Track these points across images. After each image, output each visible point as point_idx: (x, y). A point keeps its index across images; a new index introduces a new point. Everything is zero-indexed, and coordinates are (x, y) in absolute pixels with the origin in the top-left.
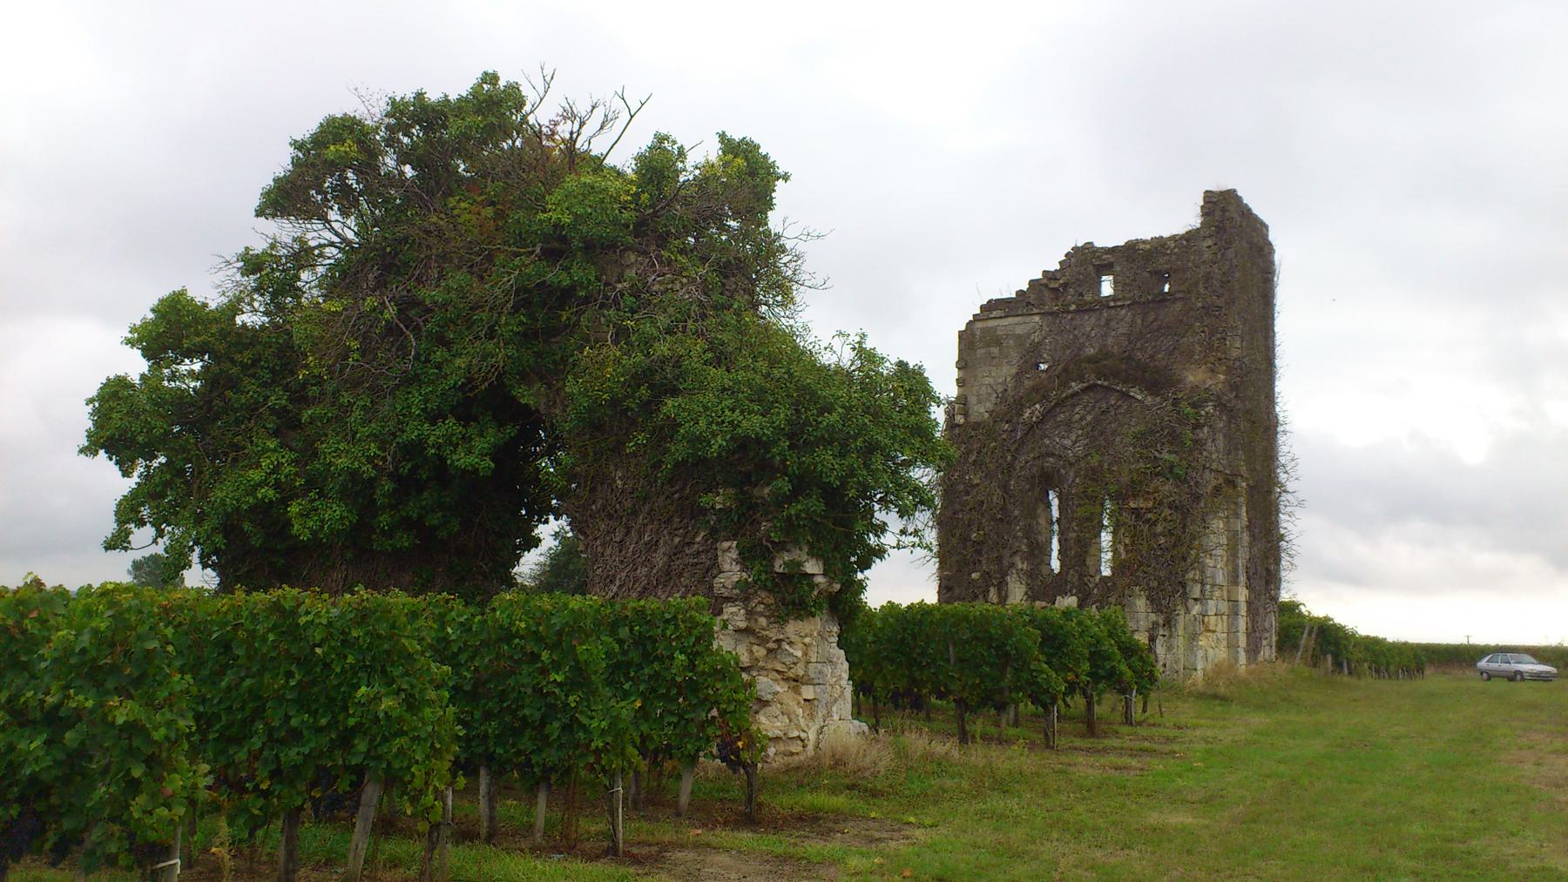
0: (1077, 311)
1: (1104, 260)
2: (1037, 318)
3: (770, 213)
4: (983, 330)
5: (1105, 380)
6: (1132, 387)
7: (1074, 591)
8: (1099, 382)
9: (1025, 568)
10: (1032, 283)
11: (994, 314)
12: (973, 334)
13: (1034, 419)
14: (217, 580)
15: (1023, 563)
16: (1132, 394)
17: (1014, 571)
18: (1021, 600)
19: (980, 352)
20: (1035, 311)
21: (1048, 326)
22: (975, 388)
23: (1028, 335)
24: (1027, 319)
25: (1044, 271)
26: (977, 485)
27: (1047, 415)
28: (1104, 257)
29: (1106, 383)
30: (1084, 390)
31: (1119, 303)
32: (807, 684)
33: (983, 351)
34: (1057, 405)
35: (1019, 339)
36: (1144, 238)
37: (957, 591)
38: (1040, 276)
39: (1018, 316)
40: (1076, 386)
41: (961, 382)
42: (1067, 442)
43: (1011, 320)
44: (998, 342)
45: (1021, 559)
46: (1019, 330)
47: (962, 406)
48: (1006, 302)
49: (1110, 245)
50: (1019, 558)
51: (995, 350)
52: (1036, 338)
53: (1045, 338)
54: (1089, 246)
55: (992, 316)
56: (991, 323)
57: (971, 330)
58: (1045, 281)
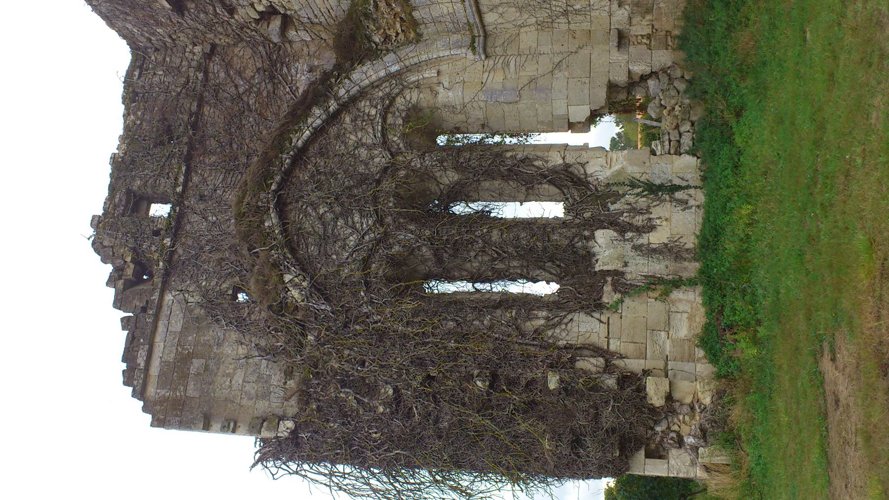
0: (175, 238)
1: (121, 200)
2: (168, 297)
3: (100, 212)
4: (161, 384)
5: (272, 178)
6: (291, 143)
7: (586, 233)
8: (273, 187)
9: (544, 314)
10: (119, 303)
11: (141, 361)
12: (163, 401)
13: (305, 284)
14: (334, 61)
15: (537, 318)
16: (300, 143)
17: (550, 333)
18: (601, 322)
19: (192, 391)
20: (156, 297)
21: (183, 281)
22: (244, 402)
23: (188, 310)
24: (165, 311)
25: (107, 284)
26: (396, 390)
27: (305, 267)
28: (117, 200)
29: (278, 178)
30: (282, 214)
31: (181, 179)
32: (483, 26)
33: (191, 386)
34: (293, 251)
35: (192, 323)
36: (123, 121)
37: (582, 421)
38: (112, 292)
39: (155, 327)
40: (272, 221)
41: (230, 426)
42: (352, 240)
43: (158, 338)
44: (184, 360)
45: (530, 319)
46: (177, 325)
47: (265, 424)
48: (131, 343)
49: (106, 193)
50: (528, 324)
51: (197, 364)
52: (194, 299)
53: (199, 286)
54: (97, 223)
55: (142, 365)
56: (155, 370)
57: (155, 404)
58: (120, 283)
